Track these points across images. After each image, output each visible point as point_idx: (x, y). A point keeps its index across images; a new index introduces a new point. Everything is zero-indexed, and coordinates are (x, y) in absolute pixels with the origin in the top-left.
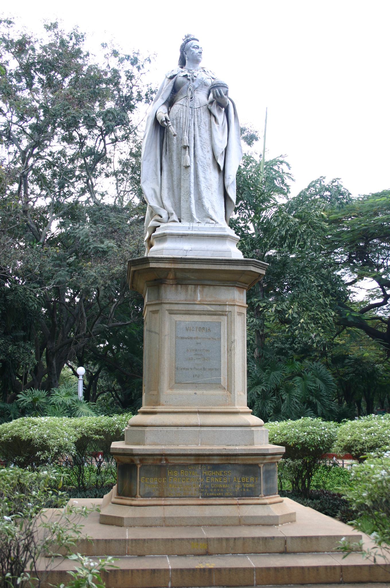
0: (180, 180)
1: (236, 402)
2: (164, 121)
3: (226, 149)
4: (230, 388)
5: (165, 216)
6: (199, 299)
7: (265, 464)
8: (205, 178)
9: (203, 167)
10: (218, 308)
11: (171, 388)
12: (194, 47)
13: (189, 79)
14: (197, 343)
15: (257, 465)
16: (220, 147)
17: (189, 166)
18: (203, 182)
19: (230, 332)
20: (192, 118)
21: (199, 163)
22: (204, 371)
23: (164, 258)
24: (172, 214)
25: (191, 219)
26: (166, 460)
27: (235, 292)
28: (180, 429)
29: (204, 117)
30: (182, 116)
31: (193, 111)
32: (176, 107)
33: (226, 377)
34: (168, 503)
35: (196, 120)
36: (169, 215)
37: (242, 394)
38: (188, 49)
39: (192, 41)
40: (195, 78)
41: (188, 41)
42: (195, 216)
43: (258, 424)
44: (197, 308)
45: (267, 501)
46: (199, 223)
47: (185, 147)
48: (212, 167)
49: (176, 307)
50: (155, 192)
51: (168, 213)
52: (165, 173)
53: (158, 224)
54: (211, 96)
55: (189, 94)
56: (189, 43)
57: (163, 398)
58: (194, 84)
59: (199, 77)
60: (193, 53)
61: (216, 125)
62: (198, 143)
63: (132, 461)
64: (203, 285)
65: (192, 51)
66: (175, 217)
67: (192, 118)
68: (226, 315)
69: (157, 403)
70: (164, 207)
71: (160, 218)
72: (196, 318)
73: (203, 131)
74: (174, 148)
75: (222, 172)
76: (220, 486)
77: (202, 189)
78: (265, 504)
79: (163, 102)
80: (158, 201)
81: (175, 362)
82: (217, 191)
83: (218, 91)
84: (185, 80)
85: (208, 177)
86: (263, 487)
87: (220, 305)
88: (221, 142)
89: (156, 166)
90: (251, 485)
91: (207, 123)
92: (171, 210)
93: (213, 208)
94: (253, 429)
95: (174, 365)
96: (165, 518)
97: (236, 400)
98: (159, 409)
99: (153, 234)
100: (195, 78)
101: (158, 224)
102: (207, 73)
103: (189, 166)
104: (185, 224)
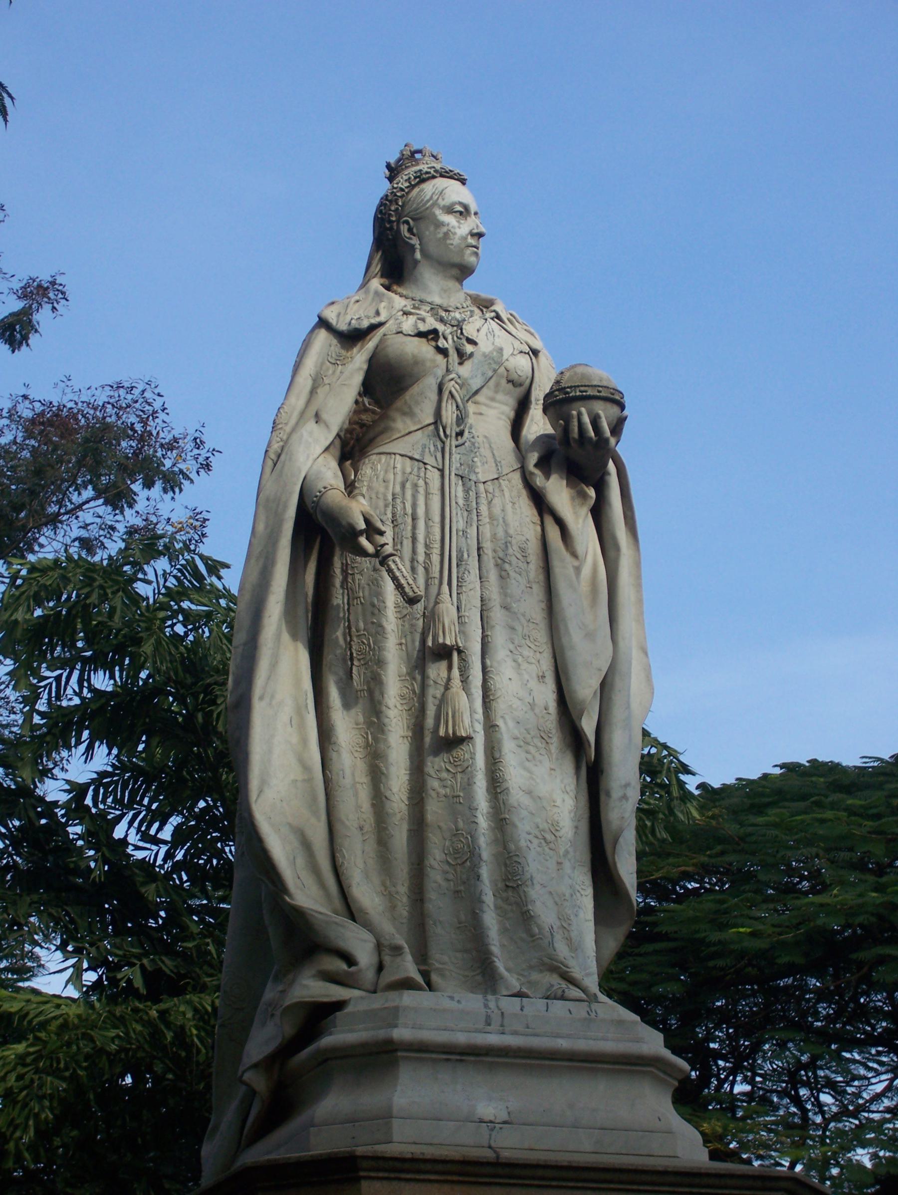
12: (449, 210)
13: (443, 352)
23: (403, 1160)
24: (397, 950)
25: (485, 976)
31: (472, 494)
36: (384, 949)
38: (422, 217)
39: (441, 182)
40: (469, 348)
41: (423, 181)
46: (519, 995)
50: (306, 845)
51: (379, 947)
53: (337, 993)
56: (429, 188)
58: (465, 370)
59: (485, 346)
60: (446, 235)
65: (442, 224)
66: (410, 968)
67: (468, 523)
71: (344, 966)
73: (517, 584)
77: (523, 843)
80: (322, 885)
83: (586, 419)
84: (425, 349)
100: (469, 348)
101: (337, 993)
103: (469, 738)
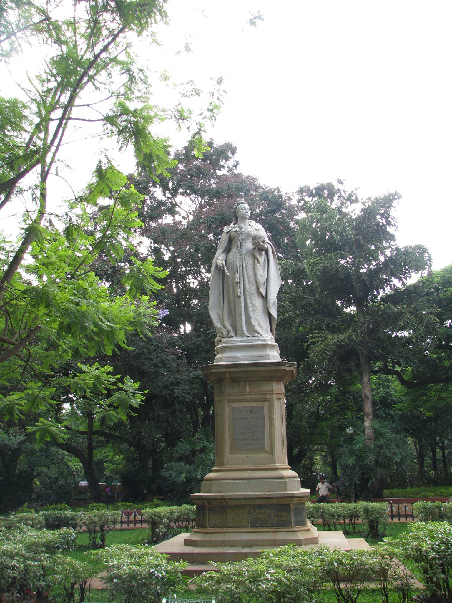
0: (235, 305)
3: (267, 280)
4: (272, 452)
5: (225, 333)
6: (248, 391)
7: (294, 504)
8: (252, 304)
9: (250, 296)
10: (262, 396)
11: (231, 453)
12: (242, 209)
15: (288, 505)
16: (262, 279)
17: (240, 297)
19: (271, 413)
22: (254, 439)
25: (243, 335)
26: (225, 502)
27: (273, 384)
28: (236, 481)
29: (250, 261)
32: (231, 254)
34: (228, 531)
36: (228, 332)
42: (245, 332)
44: (247, 397)
45: (296, 529)
47: (237, 283)
48: (256, 295)
49: (232, 398)
52: (225, 302)
53: (221, 339)
55: (239, 244)
57: (225, 461)
58: (243, 236)
61: (258, 265)
62: (246, 279)
63: (204, 504)
64: (251, 381)
66: (232, 334)
69: (222, 464)
72: (247, 404)
74: (230, 283)
75: (265, 298)
76: (263, 519)
78: (294, 531)
82: (262, 312)
84: (236, 234)
85: (254, 303)
86: (293, 519)
88: (262, 276)
89: (219, 297)
90: (284, 519)
92: (230, 328)
94: (287, 480)
96: (224, 541)
98: (223, 468)
103: (240, 297)
104: (239, 339)
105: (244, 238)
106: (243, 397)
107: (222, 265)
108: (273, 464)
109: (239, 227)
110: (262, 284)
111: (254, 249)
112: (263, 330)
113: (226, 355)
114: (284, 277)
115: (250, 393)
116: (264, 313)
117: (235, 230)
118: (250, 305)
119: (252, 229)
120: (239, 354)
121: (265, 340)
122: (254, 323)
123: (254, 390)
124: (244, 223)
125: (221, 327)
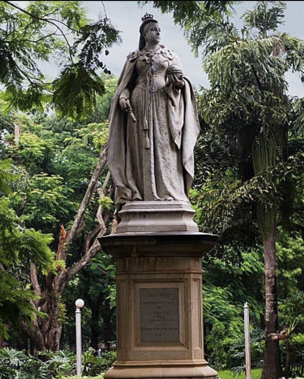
1: (193, 357)
2: (125, 108)
4: (187, 344)
5: (129, 194)
8: (164, 158)
9: (162, 148)
10: (177, 276)
14: (159, 307)
16: (177, 128)
18: (161, 162)
19: (187, 296)
20: (150, 102)
21: (158, 145)
27: (191, 261)
30: (141, 101)
32: (137, 91)
33: (184, 336)
35: (154, 104)
36: (133, 193)
37: (199, 348)
42: (155, 194)
43: (213, 374)
44: (158, 277)
47: (145, 130)
49: (139, 277)
52: (128, 154)
54: (167, 79)
61: (173, 108)
66: (138, 196)
67: (150, 102)
68: (183, 282)
70: (128, 186)
75: (180, 152)
77: (161, 169)
79: (125, 86)
81: (141, 323)
82: (176, 168)
84: (144, 64)
87: (178, 273)
88: (177, 123)
91: (164, 106)
92: (135, 188)
93: (172, 184)
95: (139, 326)
97: (193, 354)
99: (120, 212)
102: (165, 55)
105: (155, 70)
106: (153, 277)
107: (127, 105)
108: (189, 359)
109: (147, 55)
110: (177, 133)
111: (168, 85)
112: (176, 191)
113: (132, 223)
114: (203, 126)
115: (161, 272)
116: (178, 170)
117: (141, 58)
118: (161, 160)
119: (165, 59)
120: (148, 222)
121: (180, 206)
122: (167, 183)
123: (167, 269)
124: (153, 48)
125: (123, 186)
